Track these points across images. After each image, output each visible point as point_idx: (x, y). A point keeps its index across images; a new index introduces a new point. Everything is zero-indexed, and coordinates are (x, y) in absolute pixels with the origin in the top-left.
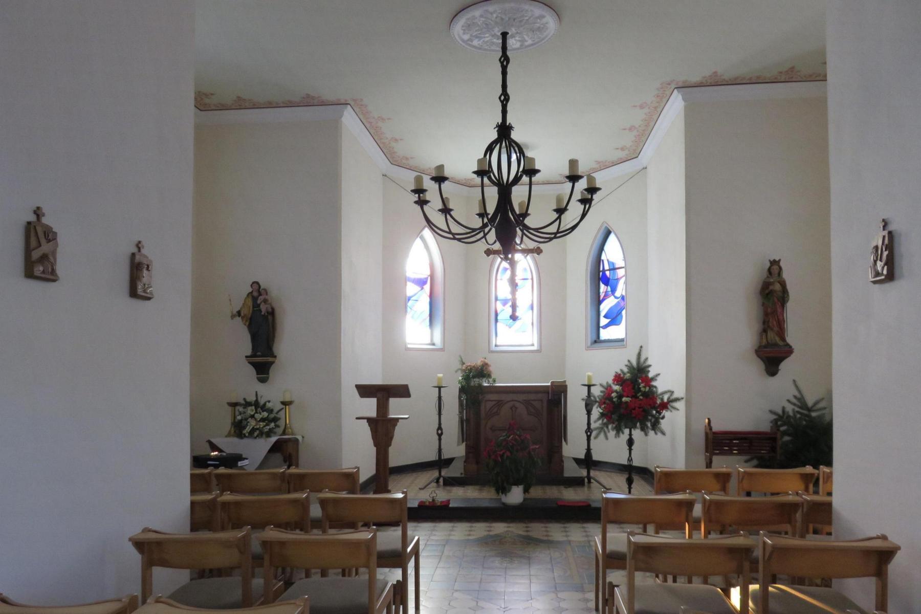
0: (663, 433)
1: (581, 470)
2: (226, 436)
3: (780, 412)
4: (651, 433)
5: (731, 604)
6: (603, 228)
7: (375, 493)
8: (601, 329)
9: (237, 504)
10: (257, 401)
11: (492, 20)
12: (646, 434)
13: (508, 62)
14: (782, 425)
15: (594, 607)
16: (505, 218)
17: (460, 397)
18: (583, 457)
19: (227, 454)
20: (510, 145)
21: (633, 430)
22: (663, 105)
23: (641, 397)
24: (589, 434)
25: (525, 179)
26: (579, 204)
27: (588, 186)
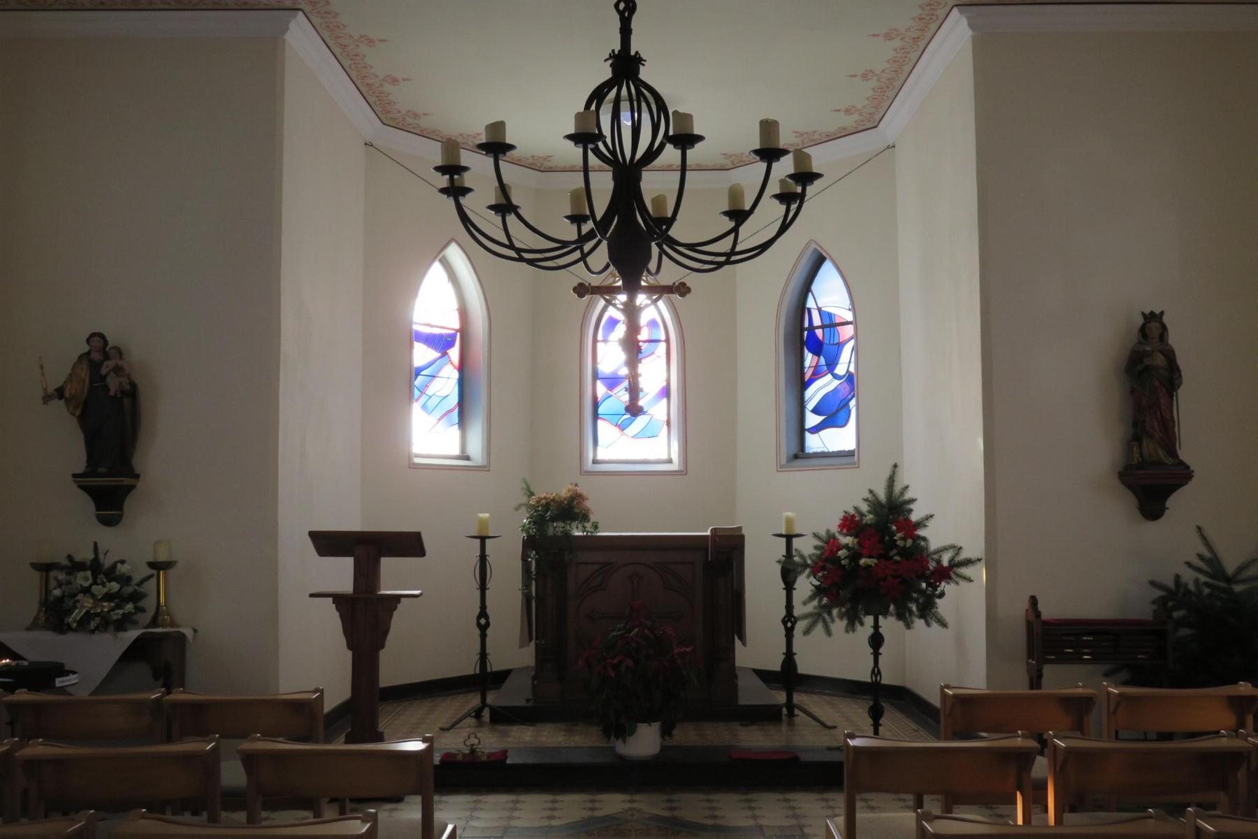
0: (943, 624)
2: (28, 629)
3: (1171, 584)
4: (919, 623)
7: (347, 742)
8: (808, 435)
9: (60, 763)
10: (96, 560)
14: (1175, 608)
17: (525, 557)
18: (777, 668)
19: (31, 663)
20: (639, 93)
21: (880, 617)
23: (897, 558)
25: (671, 154)
26: (776, 202)
27: (795, 170)
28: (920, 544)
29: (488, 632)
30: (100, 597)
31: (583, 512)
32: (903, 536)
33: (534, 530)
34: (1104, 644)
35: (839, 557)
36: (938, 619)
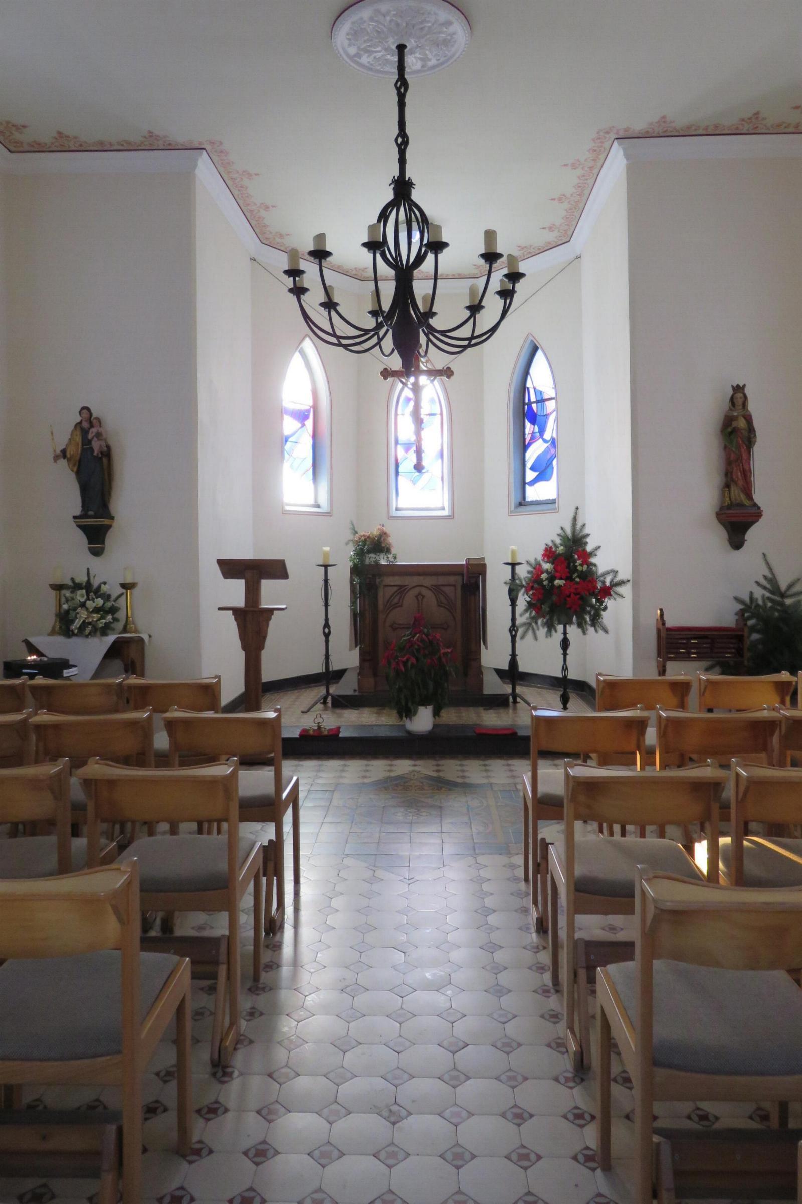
1: (505, 685)
3: (747, 600)
4: (591, 630)
5: (695, 865)
6: (528, 342)
8: (527, 486)
9: (56, 727)
10: (88, 582)
11: (385, 26)
12: (584, 633)
13: (406, 89)
14: (749, 618)
15: (522, 876)
16: (405, 314)
17: (352, 581)
22: (599, 164)
23: (578, 580)
24: (514, 633)
26: (498, 297)
28: (592, 569)
29: (330, 638)
30: (91, 610)
31: (387, 546)
32: (581, 563)
33: (358, 561)
34: (705, 646)
35: (542, 579)
36: (603, 627)
